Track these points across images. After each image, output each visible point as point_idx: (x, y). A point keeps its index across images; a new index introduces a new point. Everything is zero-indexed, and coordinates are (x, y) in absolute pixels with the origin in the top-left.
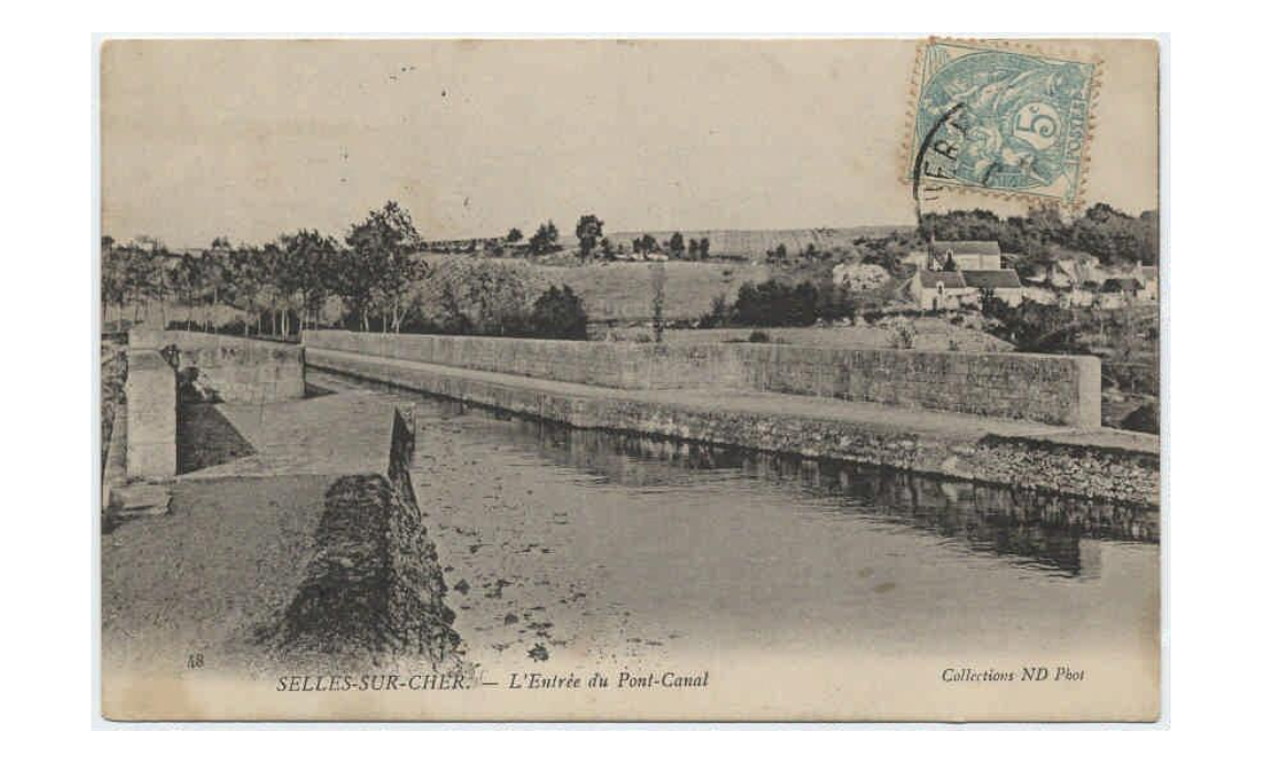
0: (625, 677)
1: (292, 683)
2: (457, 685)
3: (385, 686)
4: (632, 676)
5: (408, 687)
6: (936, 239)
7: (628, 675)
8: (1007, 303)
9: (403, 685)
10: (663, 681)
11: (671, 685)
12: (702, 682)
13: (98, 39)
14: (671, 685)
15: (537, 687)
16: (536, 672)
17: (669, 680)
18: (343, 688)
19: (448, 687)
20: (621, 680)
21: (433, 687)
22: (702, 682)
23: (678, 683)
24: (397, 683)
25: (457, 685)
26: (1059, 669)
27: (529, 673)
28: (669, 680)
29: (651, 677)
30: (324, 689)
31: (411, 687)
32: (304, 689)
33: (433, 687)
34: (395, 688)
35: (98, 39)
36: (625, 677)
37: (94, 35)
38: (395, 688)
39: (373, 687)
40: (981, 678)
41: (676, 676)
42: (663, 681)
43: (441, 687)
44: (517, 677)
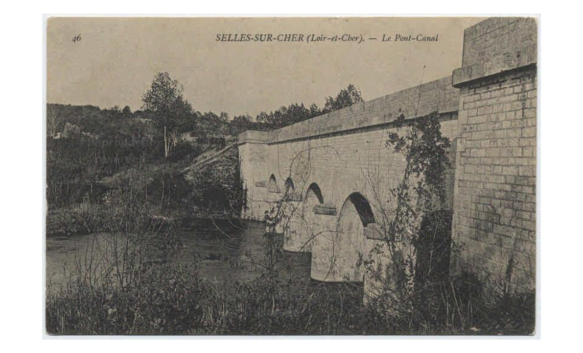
0: (398, 36)
1: (223, 37)
2: (300, 40)
3: (266, 39)
4: (401, 36)
5: (341, 40)
6: (416, 237)
7: (400, 36)
8: (306, 258)
9: (275, 39)
10: (278, 38)
11: (421, 40)
12: (435, 39)
13: (46, 17)
14: (421, 40)
15: (226, 40)
16: (295, 33)
17: (420, 38)
18: (247, 40)
19: (226, 40)
20: (396, 38)
21: (289, 40)
22: (435, 39)
23: (424, 39)
24: (271, 38)
25: (300, 40)
26: (397, 35)
27: (288, 34)
28: (420, 38)
29: (336, 37)
30: (232, 40)
31: (343, 40)
32: (229, 40)
33: (289, 40)
34: (271, 40)
35: (46, 17)
36: (398, 36)
37: (43, 15)
38: (271, 40)
39: (261, 40)
40: (233, 37)
41: (423, 36)
42: (278, 38)
43: (293, 40)
44: (231, 36)
